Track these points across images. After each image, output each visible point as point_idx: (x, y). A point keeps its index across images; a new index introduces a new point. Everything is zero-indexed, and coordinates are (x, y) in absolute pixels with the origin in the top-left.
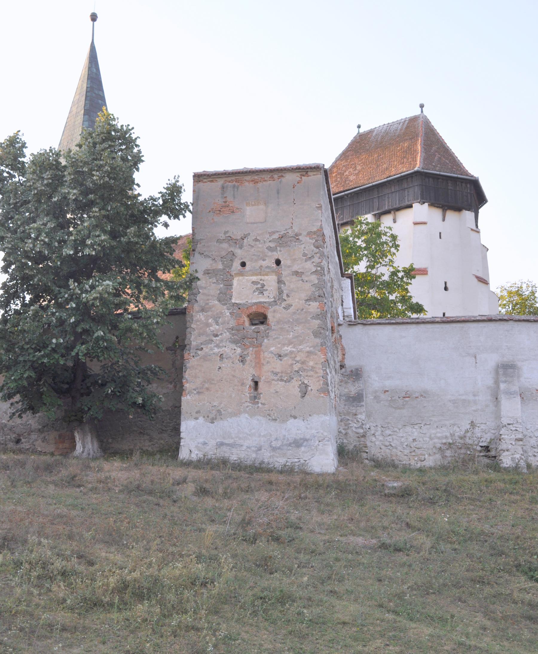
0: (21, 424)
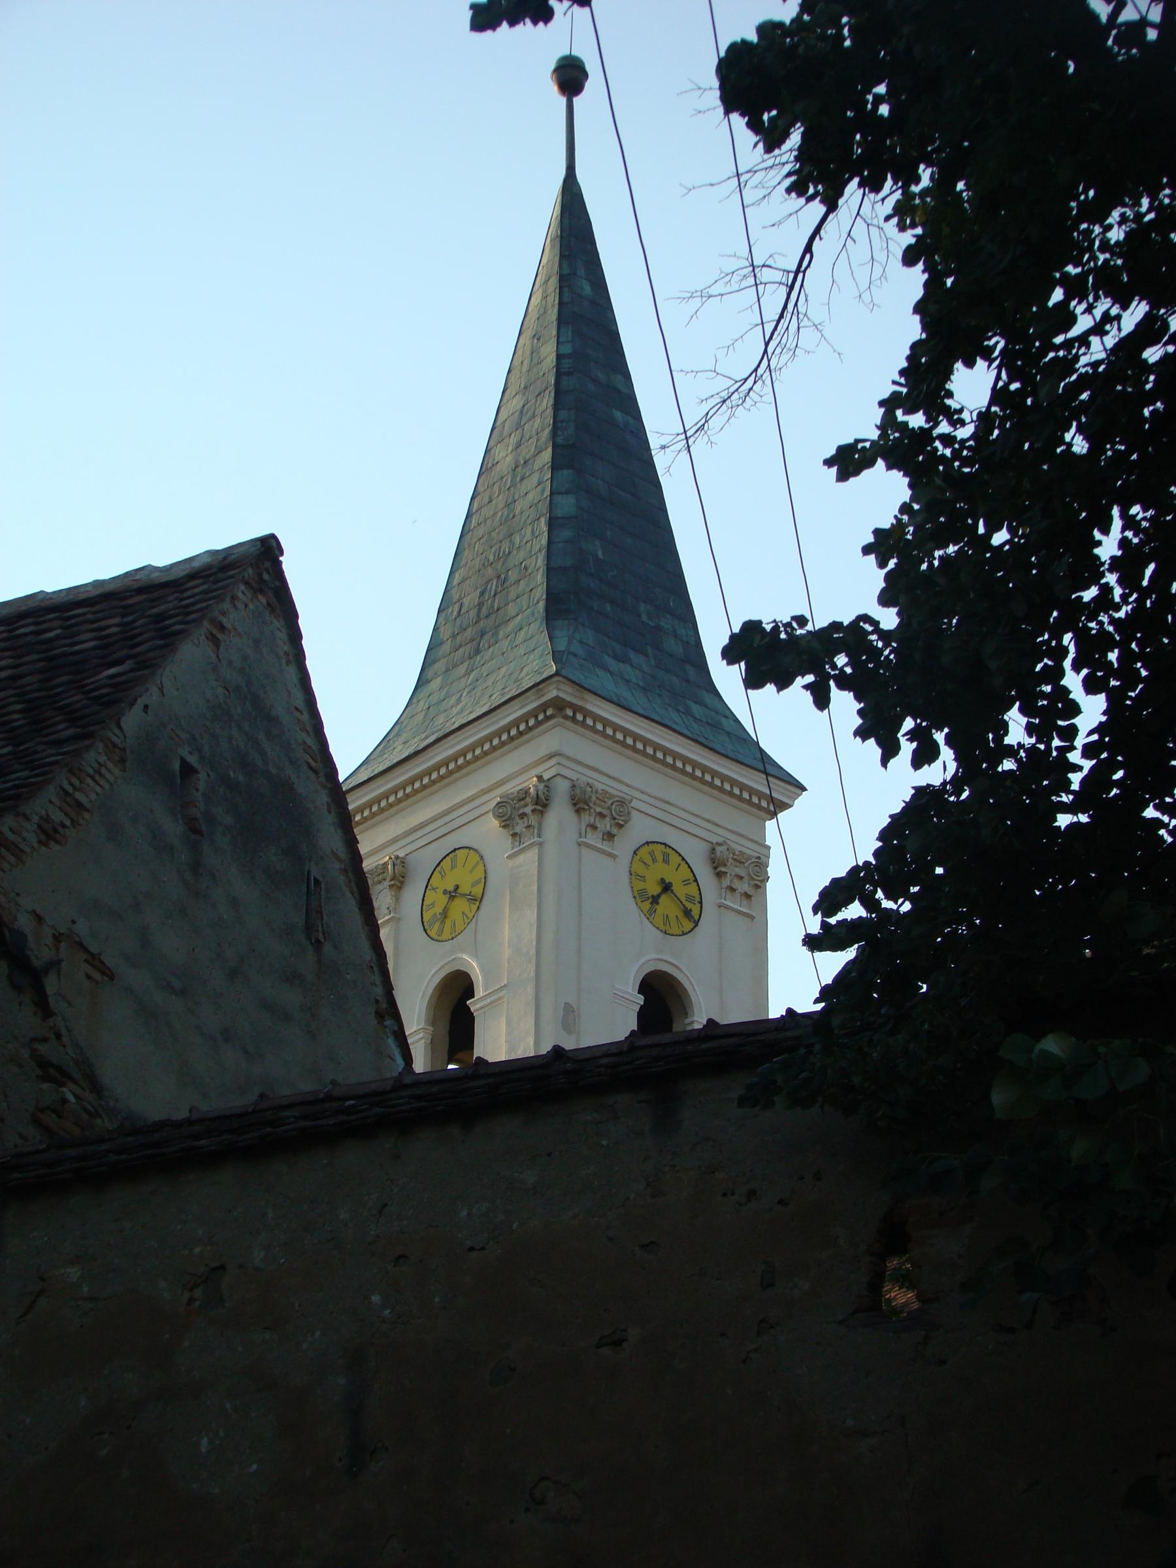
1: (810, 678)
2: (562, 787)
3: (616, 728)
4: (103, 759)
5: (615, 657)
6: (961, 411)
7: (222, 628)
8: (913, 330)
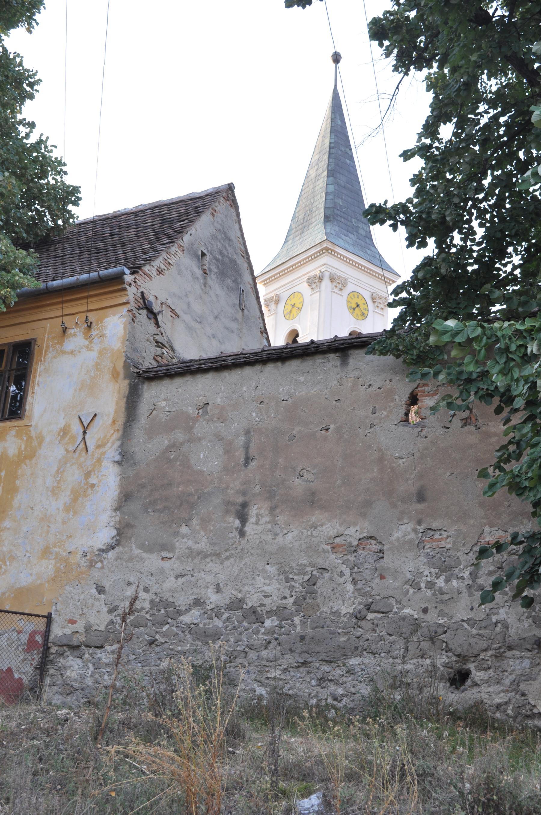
0: (468, 621)
1: (392, 222)
2: (327, 274)
3: (344, 256)
4: (177, 250)
5: (344, 235)
6: (442, 139)
7: (215, 211)
8: (428, 112)
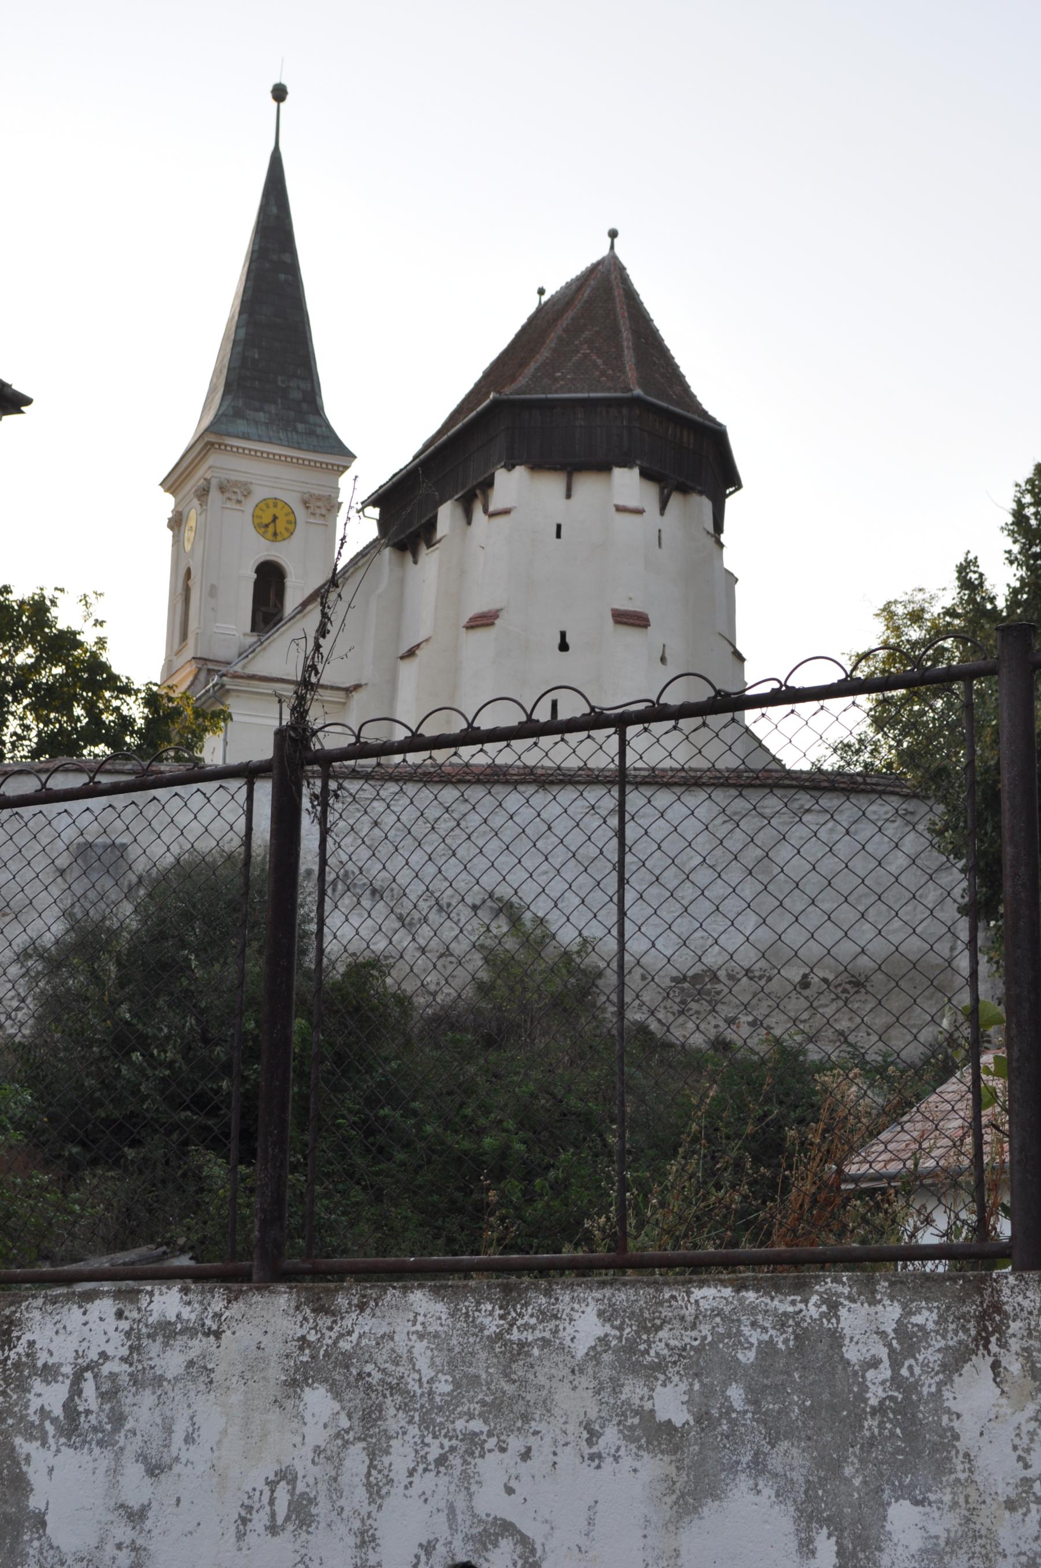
2: (214, 483)
